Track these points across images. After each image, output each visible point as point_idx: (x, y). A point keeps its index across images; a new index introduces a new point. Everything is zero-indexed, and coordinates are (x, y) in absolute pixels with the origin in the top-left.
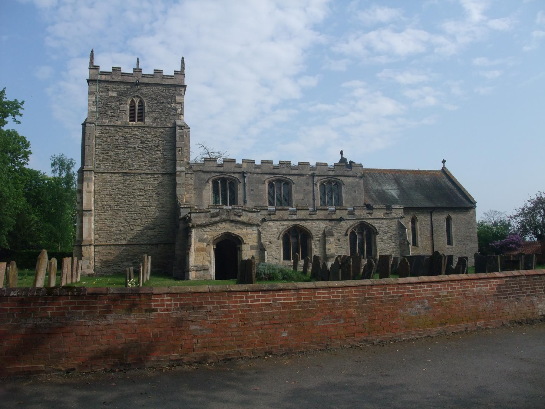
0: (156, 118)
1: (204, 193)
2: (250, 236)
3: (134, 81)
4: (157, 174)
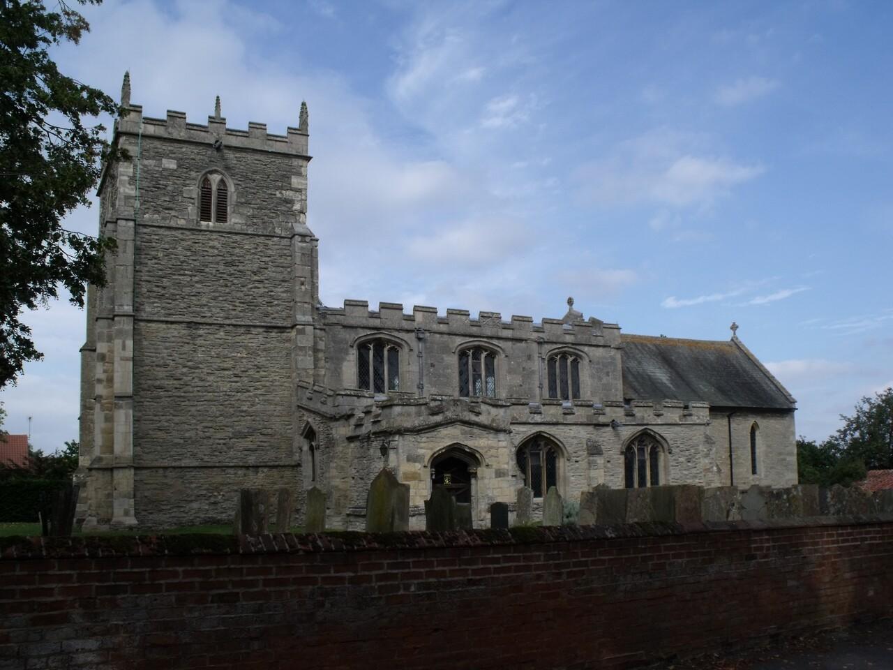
0: (254, 217)
1: (344, 368)
2: (493, 452)
3: (212, 141)
4: (255, 327)
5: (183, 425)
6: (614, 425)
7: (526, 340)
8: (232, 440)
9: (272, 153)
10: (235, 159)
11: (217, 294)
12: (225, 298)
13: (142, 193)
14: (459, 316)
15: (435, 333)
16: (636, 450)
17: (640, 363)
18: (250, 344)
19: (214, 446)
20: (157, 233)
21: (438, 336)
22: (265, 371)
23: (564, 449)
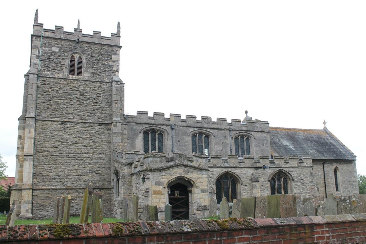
0: (94, 73)
1: (136, 142)
2: (200, 180)
3: (76, 39)
4: (94, 123)
5: (58, 169)
6: (264, 167)
7: (223, 129)
8: (81, 176)
9: (103, 44)
10: (86, 47)
11: (76, 108)
12: (80, 110)
13: (42, 62)
14: (191, 118)
15: (180, 126)
16: (276, 180)
17: (279, 140)
18: (91, 131)
19: (73, 179)
20: (48, 80)
21: (182, 127)
22: (98, 144)
23: (239, 179)
